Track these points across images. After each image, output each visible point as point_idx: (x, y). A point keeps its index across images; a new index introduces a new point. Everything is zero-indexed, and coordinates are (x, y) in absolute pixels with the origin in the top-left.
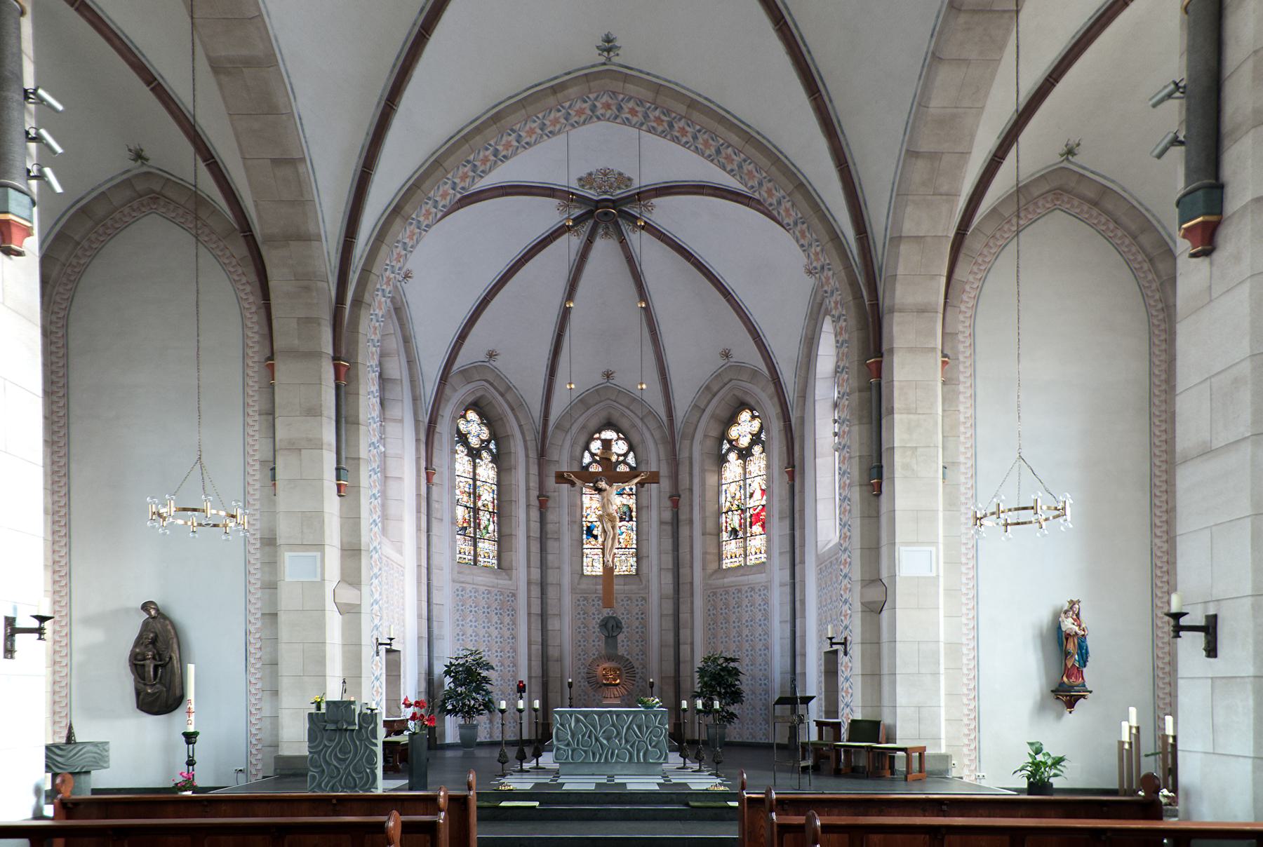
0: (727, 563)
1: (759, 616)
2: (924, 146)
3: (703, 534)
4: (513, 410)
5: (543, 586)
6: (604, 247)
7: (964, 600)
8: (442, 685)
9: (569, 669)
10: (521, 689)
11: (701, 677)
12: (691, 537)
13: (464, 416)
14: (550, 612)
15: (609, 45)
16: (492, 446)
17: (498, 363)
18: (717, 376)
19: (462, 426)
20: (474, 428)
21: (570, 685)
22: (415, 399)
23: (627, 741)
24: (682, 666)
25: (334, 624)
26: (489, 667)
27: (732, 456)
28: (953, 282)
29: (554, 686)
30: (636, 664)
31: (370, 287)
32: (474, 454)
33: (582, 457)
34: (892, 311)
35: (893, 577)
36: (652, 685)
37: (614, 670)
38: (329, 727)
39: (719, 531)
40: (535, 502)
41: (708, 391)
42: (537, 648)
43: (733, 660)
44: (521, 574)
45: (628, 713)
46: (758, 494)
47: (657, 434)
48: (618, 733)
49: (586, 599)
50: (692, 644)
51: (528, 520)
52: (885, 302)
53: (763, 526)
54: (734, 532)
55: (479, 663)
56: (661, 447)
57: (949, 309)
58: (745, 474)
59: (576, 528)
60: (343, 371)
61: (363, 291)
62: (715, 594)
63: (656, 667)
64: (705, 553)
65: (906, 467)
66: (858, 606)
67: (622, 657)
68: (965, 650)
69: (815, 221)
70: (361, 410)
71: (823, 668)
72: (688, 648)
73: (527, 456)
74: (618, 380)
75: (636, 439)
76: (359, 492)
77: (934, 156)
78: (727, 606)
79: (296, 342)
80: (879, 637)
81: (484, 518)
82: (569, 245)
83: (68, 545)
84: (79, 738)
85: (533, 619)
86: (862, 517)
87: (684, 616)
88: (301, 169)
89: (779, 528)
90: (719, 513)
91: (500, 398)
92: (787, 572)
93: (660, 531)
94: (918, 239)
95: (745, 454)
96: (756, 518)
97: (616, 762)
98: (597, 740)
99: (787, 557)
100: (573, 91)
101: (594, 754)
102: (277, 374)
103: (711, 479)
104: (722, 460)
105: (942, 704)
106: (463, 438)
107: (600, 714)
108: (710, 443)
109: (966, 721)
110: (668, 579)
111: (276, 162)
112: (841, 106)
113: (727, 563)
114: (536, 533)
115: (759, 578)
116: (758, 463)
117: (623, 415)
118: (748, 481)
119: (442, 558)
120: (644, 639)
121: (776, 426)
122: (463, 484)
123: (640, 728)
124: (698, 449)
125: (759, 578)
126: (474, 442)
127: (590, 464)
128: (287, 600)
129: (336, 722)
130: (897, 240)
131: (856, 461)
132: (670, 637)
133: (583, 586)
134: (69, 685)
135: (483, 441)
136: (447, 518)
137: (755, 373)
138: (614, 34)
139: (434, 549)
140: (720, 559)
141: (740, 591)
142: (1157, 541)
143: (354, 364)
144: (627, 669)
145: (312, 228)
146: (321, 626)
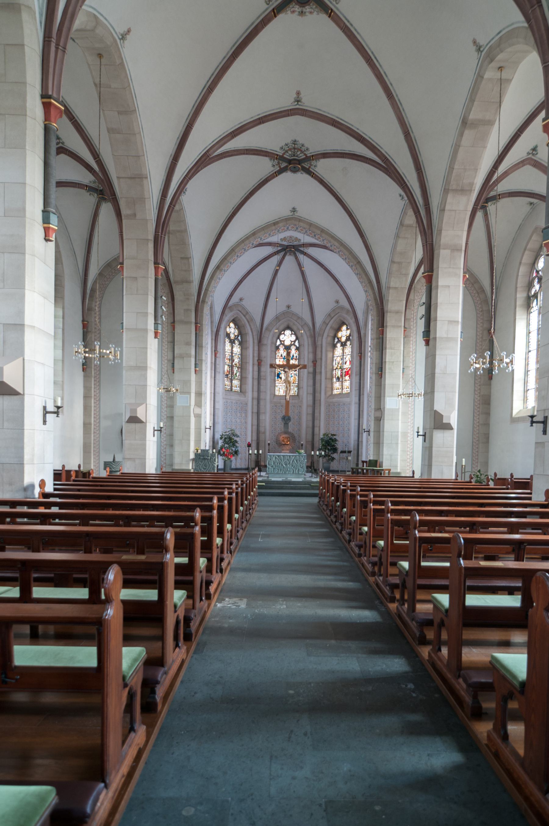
0: (335, 392)
2: (396, 259)
3: (326, 379)
4: (248, 322)
5: (258, 400)
6: (289, 260)
7: (409, 416)
8: (218, 443)
9: (268, 437)
10: (249, 445)
11: (322, 442)
12: (321, 380)
13: (229, 325)
14: (261, 412)
15: (294, 210)
16: (239, 338)
17: (243, 303)
18: (334, 310)
19: (228, 330)
20: (232, 330)
21: (269, 444)
22: (212, 322)
24: (315, 436)
25: (193, 420)
26: (238, 436)
27: (339, 345)
28: (409, 299)
29: (262, 444)
30: (296, 435)
31: (208, 296)
32: (232, 342)
33: (276, 342)
34: (387, 312)
35: (384, 408)
36: (302, 445)
37: (287, 438)
38: (201, 458)
39: (332, 377)
40: (256, 363)
41: (330, 316)
42: (255, 427)
43: (335, 435)
44: (250, 395)
45: (293, 456)
46: (348, 363)
47: (308, 334)
49: (276, 406)
50: (319, 427)
51: (253, 371)
52: (385, 309)
53: (349, 376)
54: (338, 379)
55: (234, 435)
56: (309, 339)
57: (407, 310)
58: (343, 353)
59: (273, 374)
60: (198, 328)
61: (205, 297)
62: (329, 405)
63: (304, 436)
64: (326, 387)
65: (390, 369)
66: (373, 418)
67: (290, 433)
68: (409, 435)
69: (364, 276)
70: (204, 341)
73: (254, 342)
74: (293, 309)
75: (299, 335)
76: (202, 372)
77: (399, 263)
78: (334, 411)
79: (183, 318)
80: (380, 430)
81: (235, 370)
82: (275, 259)
83: (99, 389)
84: (117, 460)
85: (254, 415)
86: (376, 385)
88: (190, 260)
89: (356, 379)
90: (333, 370)
91: (243, 317)
92: (357, 398)
93: (308, 377)
94: (396, 288)
95: (344, 345)
96: (347, 373)
99: (358, 392)
100: (281, 225)
102: (176, 330)
103: (330, 355)
104: (334, 346)
105: (399, 454)
106: (228, 335)
107: (283, 456)
108: (330, 339)
109: (408, 460)
110: (310, 398)
111: (182, 258)
112: (371, 241)
113: (335, 392)
114: (256, 376)
115: (347, 400)
116: (348, 350)
117: (294, 324)
118: (345, 357)
119: (220, 389)
120: (300, 424)
121: (355, 335)
122: (228, 355)
123: (297, 461)
124: (325, 341)
125: (347, 400)
126: (232, 336)
127: (279, 345)
128: (178, 412)
129: (203, 456)
130: (389, 288)
131: (374, 364)
133: (275, 400)
134: (99, 441)
135: (235, 336)
136: (221, 372)
137: (348, 311)
138: (296, 207)
139: (217, 385)
140: (332, 390)
141: (339, 405)
142: (476, 396)
143: (202, 325)
144: (292, 438)
145: (191, 279)
146: (189, 422)
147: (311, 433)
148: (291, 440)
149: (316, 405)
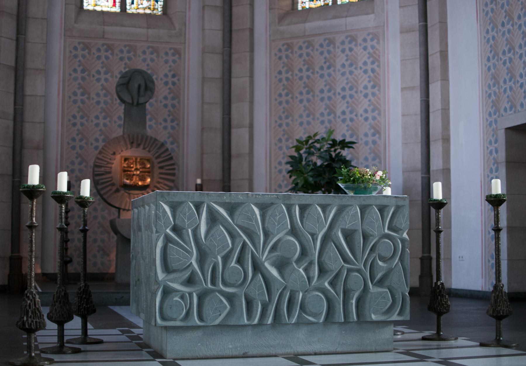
1: (364, 80)
14: (30, 64)
23: (322, 271)
48: (304, 252)
49: (86, 47)
50: (251, 126)
62: (289, 47)
71: (502, 155)
72: (244, 133)
78: (310, 67)
87: (239, 82)
97: (298, 324)
98: (257, 267)
101: (249, 303)
123: (349, 236)
132: (216, 116)
141: (331, 42)
147: (218, 151)
148: (157, 171)
149: (235, 47)
